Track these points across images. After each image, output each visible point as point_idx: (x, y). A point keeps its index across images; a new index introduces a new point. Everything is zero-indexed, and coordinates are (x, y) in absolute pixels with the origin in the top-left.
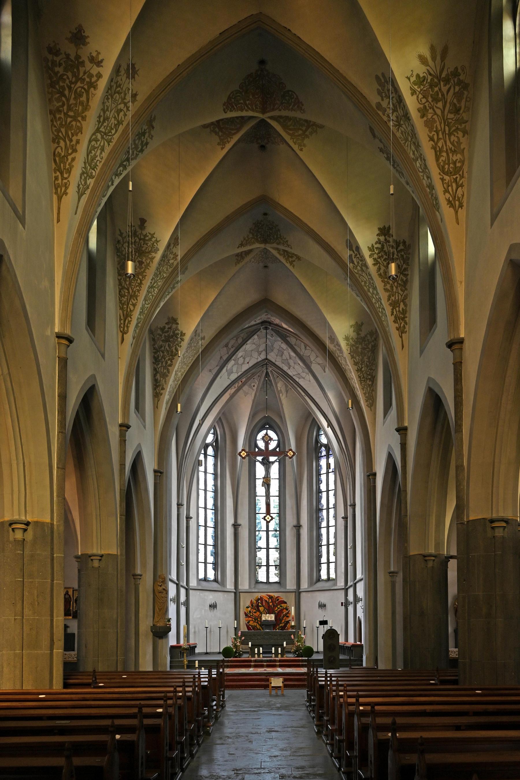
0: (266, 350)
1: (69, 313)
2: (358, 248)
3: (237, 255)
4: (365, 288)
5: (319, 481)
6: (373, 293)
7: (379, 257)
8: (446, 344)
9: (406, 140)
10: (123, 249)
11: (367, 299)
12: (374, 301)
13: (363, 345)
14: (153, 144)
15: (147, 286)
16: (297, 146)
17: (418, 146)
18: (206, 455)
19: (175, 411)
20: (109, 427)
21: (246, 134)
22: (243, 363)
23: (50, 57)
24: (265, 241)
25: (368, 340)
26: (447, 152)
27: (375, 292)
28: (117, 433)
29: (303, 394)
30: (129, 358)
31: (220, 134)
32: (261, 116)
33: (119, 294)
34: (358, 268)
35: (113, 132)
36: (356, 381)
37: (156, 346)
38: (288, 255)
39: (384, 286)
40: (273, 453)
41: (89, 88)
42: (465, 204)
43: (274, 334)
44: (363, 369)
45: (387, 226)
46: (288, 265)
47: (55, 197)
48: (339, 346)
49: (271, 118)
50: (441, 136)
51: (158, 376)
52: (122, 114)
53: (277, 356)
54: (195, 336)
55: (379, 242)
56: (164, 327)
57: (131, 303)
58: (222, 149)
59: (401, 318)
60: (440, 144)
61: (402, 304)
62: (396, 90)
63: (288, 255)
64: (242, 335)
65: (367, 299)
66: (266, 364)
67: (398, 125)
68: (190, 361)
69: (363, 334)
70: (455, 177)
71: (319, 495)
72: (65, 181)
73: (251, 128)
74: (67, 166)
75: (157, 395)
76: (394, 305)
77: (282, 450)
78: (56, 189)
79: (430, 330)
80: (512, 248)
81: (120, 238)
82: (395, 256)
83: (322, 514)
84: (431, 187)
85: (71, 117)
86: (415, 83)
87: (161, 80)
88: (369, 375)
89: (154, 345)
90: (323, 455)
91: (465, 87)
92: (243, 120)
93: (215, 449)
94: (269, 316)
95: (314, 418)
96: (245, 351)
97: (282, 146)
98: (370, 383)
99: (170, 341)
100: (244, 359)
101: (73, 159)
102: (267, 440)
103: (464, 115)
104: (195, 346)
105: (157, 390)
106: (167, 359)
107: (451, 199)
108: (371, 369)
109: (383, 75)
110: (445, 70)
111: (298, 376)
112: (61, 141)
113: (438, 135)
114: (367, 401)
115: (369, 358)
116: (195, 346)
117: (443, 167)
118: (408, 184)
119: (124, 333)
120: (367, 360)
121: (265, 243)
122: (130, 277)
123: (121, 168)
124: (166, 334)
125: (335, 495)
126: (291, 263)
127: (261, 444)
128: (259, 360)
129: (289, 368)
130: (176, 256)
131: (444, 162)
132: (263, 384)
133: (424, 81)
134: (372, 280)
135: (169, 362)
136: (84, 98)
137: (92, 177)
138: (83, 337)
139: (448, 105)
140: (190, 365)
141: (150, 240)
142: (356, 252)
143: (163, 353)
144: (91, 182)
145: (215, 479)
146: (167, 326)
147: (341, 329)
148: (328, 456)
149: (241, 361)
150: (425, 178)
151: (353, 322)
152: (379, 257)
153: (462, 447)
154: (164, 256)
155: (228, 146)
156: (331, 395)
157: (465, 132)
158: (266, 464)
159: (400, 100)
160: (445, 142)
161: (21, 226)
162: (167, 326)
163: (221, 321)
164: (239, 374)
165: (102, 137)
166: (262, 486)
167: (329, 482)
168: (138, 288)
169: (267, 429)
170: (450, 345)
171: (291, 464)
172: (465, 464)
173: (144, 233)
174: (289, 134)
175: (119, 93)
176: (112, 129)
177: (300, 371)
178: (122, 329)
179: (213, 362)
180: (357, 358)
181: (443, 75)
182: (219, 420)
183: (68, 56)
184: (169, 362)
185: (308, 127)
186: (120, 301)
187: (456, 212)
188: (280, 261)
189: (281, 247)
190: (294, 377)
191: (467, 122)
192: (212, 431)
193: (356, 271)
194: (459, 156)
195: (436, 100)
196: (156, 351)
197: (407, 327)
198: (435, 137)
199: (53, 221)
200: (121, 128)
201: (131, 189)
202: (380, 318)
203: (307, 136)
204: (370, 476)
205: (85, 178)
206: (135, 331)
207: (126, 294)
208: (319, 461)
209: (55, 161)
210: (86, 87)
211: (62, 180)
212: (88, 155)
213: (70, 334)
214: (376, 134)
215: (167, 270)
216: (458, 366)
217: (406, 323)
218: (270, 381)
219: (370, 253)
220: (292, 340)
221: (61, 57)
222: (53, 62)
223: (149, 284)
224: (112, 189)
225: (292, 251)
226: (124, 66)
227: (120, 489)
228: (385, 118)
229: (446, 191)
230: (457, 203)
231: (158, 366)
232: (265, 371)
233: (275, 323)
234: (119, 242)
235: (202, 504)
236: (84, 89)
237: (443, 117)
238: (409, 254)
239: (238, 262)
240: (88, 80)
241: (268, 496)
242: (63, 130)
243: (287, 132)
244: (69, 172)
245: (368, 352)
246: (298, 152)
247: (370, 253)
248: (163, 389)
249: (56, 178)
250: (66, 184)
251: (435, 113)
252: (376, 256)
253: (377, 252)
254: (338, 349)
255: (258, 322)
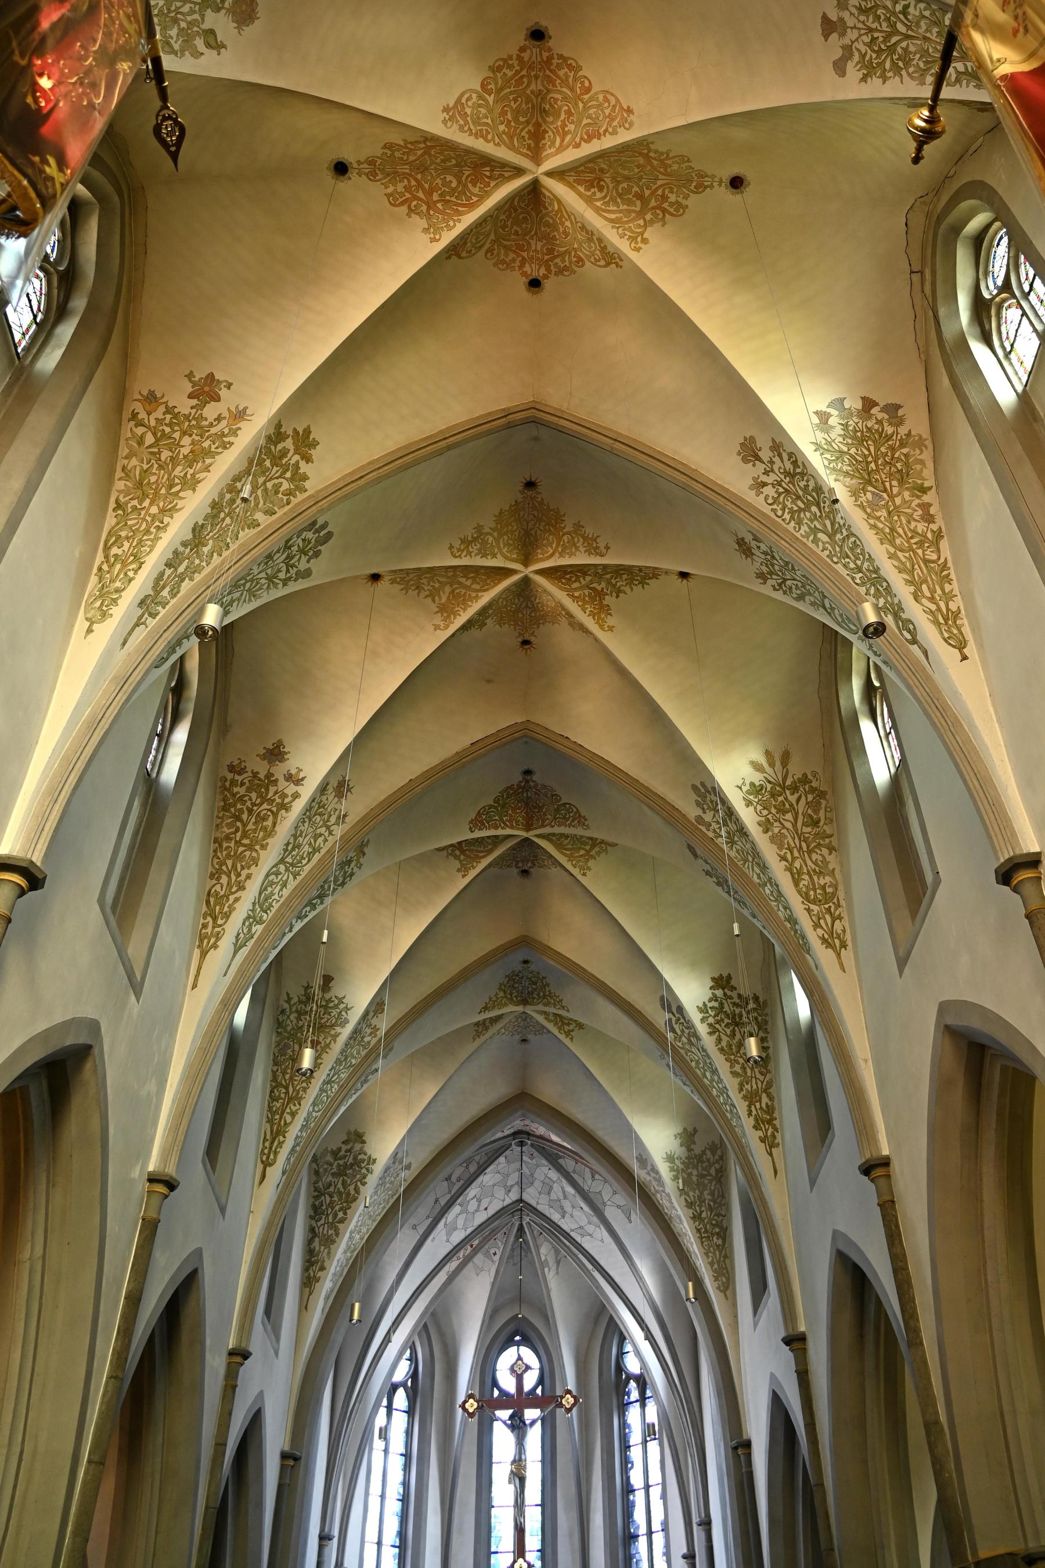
0: (521, 1184)
1: (181, 1137)
2: (680, 1009)
3: (477, 1024)
4: (697, 1071)
5: (626, 1462)
6: (712, 1080)
7: (718, 1022)
8: (860, 1168)
9: (746, 860)
10: (288, 1022)
11: (703, 1090)
12: (714, 1092)
13: (700, 1168)
14: (360, 876)
15: (321, 1081)
16: (578, 869)
17: (764, 867)
18: (390, 1408)
19: (348, 1319)
20: (208, 1356)
21: (501, 857)
22: (477, 1210)
23: (230, 776)
24: (525, 1002)
25: (708, 1160)
26: (809, 873)
27: (716, 1078)
28: (222, 1371)
29: (590, 1267)
30: (270, 1212)
31: (462, 857)
32: (524, 834)
33: (270, 1096)
34: (684, 1039)
35: (304, 862)
36: (692, 1240)
37: (320, 1184)
38: (562, 1022)
39: (731, 1067)
40: (529, 1399)
41: (278, 811)
42: (849, 943)
43: (536, 1154)
44: (704, 1215)
45: (725, 975)
46: (562, 1037)
47: (197, 952)
48: (657, 1172)
49: (538, 836)
50: (796, 854)
51: (316, 1243)
52: (320, 840)
53: (540, 1193)
54: (394, 1163)
55: (714, 998)
56: (340, 1149)
57: (288, 1110)
58: (464, 876)
59: (767, 1120)
60: (797, 864)
61: (764, 1096)
62: (724, 801)
63: (562, 1022)
64: (477, 1158)
65: (703, 1090)
66: (521, 1210)
67: (731, 842)
68: (380, 1212)
69: (697, 1151)
70: (826, 906)
71: (628, 1499)
72: (217, 929)
73: (509, 849)
74: (226, 909)
75: (309, 1282)
76: (751, 1098)
77: (548, 1393)
78: (201, 941)
79: (823, 1142)
80: (944, 1007)
81: (286, 1006)
82: (745, 1019)
83: (637, 1549)
84: (793, 920)
85: (245, 845)
86: (748, 792)
87: (382, 798)
88: (716, 1225)
89: (316, 1182)
90: (632, 1399)
91: (822, 795)
92: (496, 841)
93: (411, 1394)
94: (527, 1122)
95: (611, 1317)
96: (482, 1186)
97: (555, 870)
98: (720, 1242)
99: (346, 1175)
100: (479, 1201)
101: (237, 900)
102: (518, 1372)
103: (825, 827)
104: (392, 1183)
105: (311, 1272)
106: (337, 1208)
107: (826, 936)
108: (718, 1215)
109: (703, 784)
110: (790, 776)
111: (579, 1231)
112: (223, 876)
113: (792, 853)
114: (716, 1279)
115: (712, 1193)
116: (392, 1183)
117: (807, 894)
118: (754, 917)
119: (267, 1164)
120: (709, 1197)
121: (525, 1005)
122: (304, 1074)
123: (308, 908)
124: (341, 1162)
125: (664, 1496)
126: (568, 1034)
127: (507, 1382)
128: (506, 1203)
129: (563, 1217)
130: (376, 1029)
131: (807, 887)
132: (513, 1250)
133: (761, 789)
134: (709, 1058)
135: (341, 1215)
136: (269, 823)
137: (260, 922)
138: (195, 1180)
139: (800, 817)
140: (379, 1218)
141: (336, 1006)
142: (677, 1015)
143: (331, 1197)
144: (258, 929)
145: (407, 1467)
146: (344, 1148)
147: (658, 1139)
148: (643, 1400)
149: (473, 1206)
150: (781, 908)
151: (680, 1130)
152: (718, 1022)
153: (929, 1379)
154: (356, 1031)
155: (472, 874)
156: (645, 1268)
157: (831, 849)
158: (519, 1428)
159: (730, 812)
160: (804, 861)
161: (133, 998)
162: (344, 1148)
163: (444, 1135)
164: (469, 1231)
165: (287, 869)
166: (510, 1482)
167: (648, 1465)
168: (304, 1085)
169: (518, 1344)
170: (867, 1170)
171: (568, 1421)
172: (943, 1418)
173: (327, 996)
174: (565, 855)
175: (321, 815)
176: (303, 858)
177: (584, 1221)
178: (264, 1158)
179: (422, 1212)
180: (691, 1193)
181: (788, 782)
182: (423, 1329)
183: (255, 774)
184: (341, 1215)
185: (593, 847)
186: (270, 1108)
187: (839, 955)
188: (549, 1032)
189: (551, 1010)
190: (572, 1234)
191: (831, 836)
192: (407, 1354)
193: (680, 1044)
194: (828, 879)
195: (782, 811)
196: (317, 1192)
197: (778, 1135)
198: (789, 856)
199: (186, 986)
200: (317, 857)
201: (325, 940)
202: (728, 1122)
203: (593, 857)
204: (739, 1448)
205: (251, 925)
206: (288, 1159)
207: (283, 1095)
208: (624, 1415)
209: (208, 902)
210: (274, 809)
211: (214, 927)
212: (260, 894)
213: (174, 1174)
214: (699, 853)
215: (358, 1053)
216: (888, 1208)
217: (776, 1130)
218: (526, 1242)
219: (701, 1016)
220: (569, 1164)
221: (245, 776)
222: (233, 783)
223: (324, 1077)
224: (288, 937)
225: (570, 1015)
226: (334, 783)
227: (207, 1507)
228: (711, 835)
229: (817, 926)
230: (837, 941)
231: (319, 1224)
232: (519, 1227)
233: (538, 1133)
234: (283, 1012)
235: (371, 1535)
236: (272, 812)
237: (796, 831)
238: (766, 1015)
239: (478, 1034)
240: (279, 801)
241: (519, 1506)
242: (229, 863)
243: (562, 853)
244: (227, 916)
245: (710, 1181)
246: (579, 877)
247: (701, 1016)
248: (322, 1268)
249: (205, 926)
250: (218, 933)
251: (784, 827)
252: (711, 1020)
253: (713, 1014)
254: (654, 1178)
255: (507, 1132)
